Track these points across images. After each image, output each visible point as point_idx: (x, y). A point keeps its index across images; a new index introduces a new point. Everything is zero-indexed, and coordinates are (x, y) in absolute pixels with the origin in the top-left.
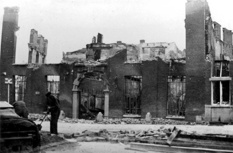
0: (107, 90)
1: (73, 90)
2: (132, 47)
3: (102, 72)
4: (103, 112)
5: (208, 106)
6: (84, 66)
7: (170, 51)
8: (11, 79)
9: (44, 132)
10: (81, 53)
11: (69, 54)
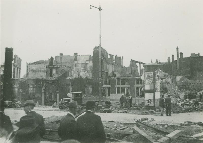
0: (58, 91)
1: (42, 91)
3: (55, 83)
4: (56, 102)
6: (47, 80)
8: (22, 90)
9: (113, 100)
11: (31, 64)
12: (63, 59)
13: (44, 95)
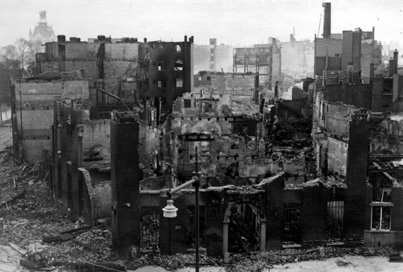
2: (239, 139)
5: (368, 231)
7: (223, 105)
10: (45, 80)
11: (23, 82)
12: (66, 49)
13: (18, 126)
